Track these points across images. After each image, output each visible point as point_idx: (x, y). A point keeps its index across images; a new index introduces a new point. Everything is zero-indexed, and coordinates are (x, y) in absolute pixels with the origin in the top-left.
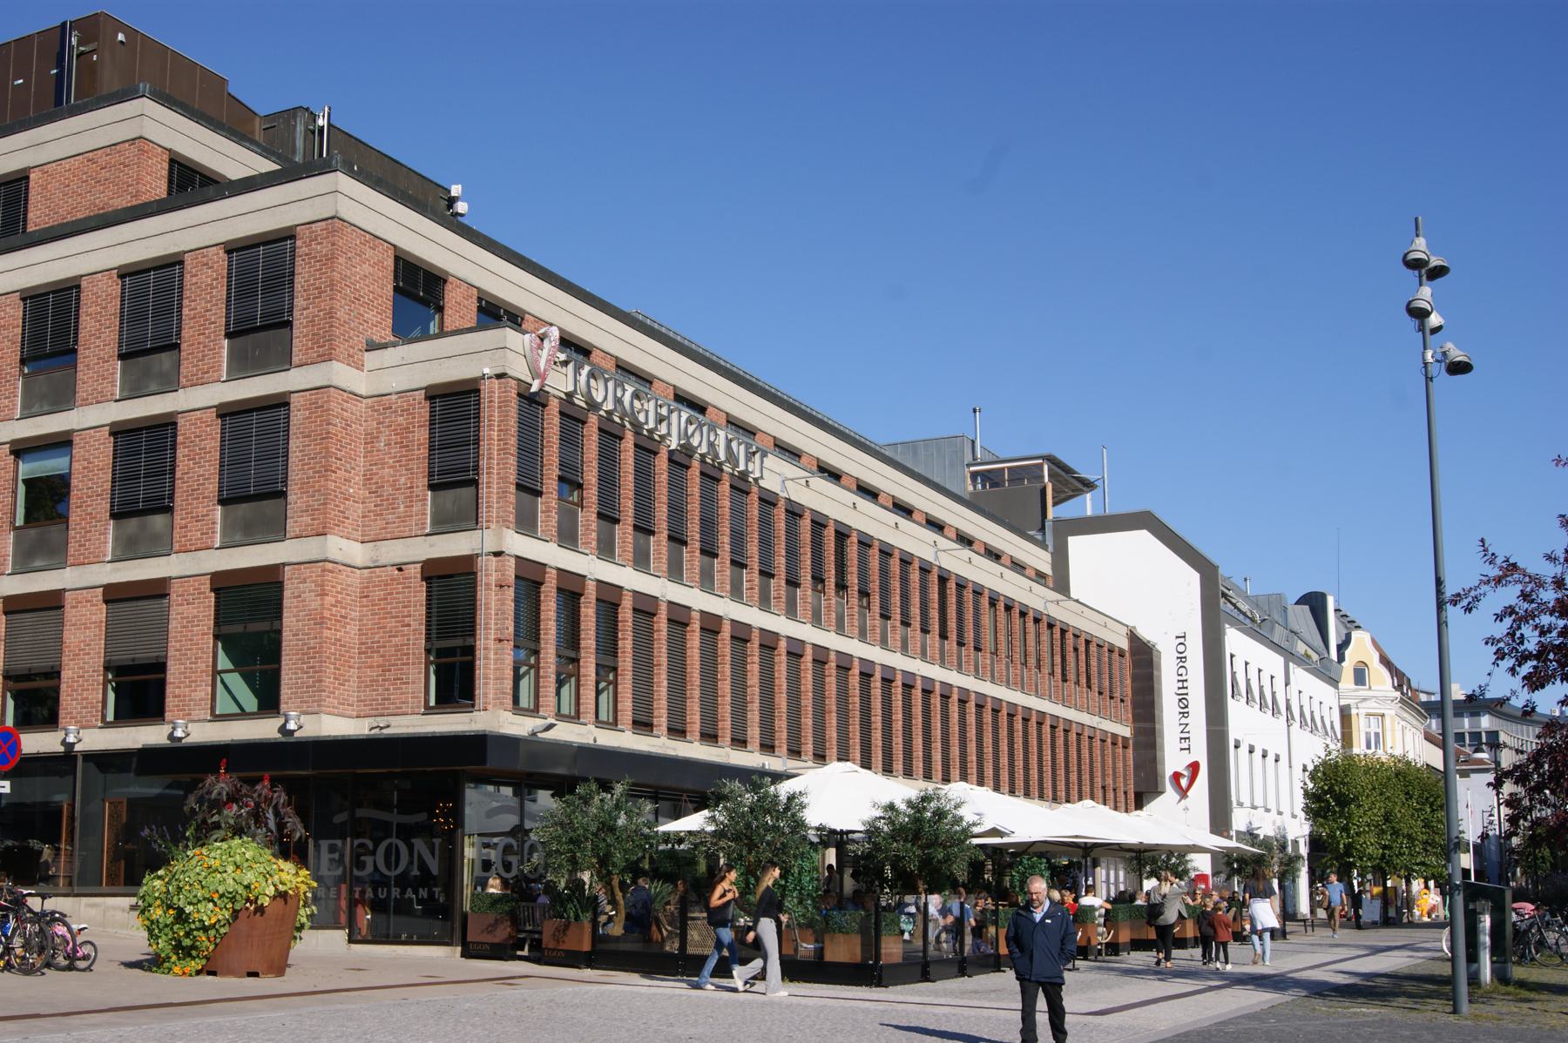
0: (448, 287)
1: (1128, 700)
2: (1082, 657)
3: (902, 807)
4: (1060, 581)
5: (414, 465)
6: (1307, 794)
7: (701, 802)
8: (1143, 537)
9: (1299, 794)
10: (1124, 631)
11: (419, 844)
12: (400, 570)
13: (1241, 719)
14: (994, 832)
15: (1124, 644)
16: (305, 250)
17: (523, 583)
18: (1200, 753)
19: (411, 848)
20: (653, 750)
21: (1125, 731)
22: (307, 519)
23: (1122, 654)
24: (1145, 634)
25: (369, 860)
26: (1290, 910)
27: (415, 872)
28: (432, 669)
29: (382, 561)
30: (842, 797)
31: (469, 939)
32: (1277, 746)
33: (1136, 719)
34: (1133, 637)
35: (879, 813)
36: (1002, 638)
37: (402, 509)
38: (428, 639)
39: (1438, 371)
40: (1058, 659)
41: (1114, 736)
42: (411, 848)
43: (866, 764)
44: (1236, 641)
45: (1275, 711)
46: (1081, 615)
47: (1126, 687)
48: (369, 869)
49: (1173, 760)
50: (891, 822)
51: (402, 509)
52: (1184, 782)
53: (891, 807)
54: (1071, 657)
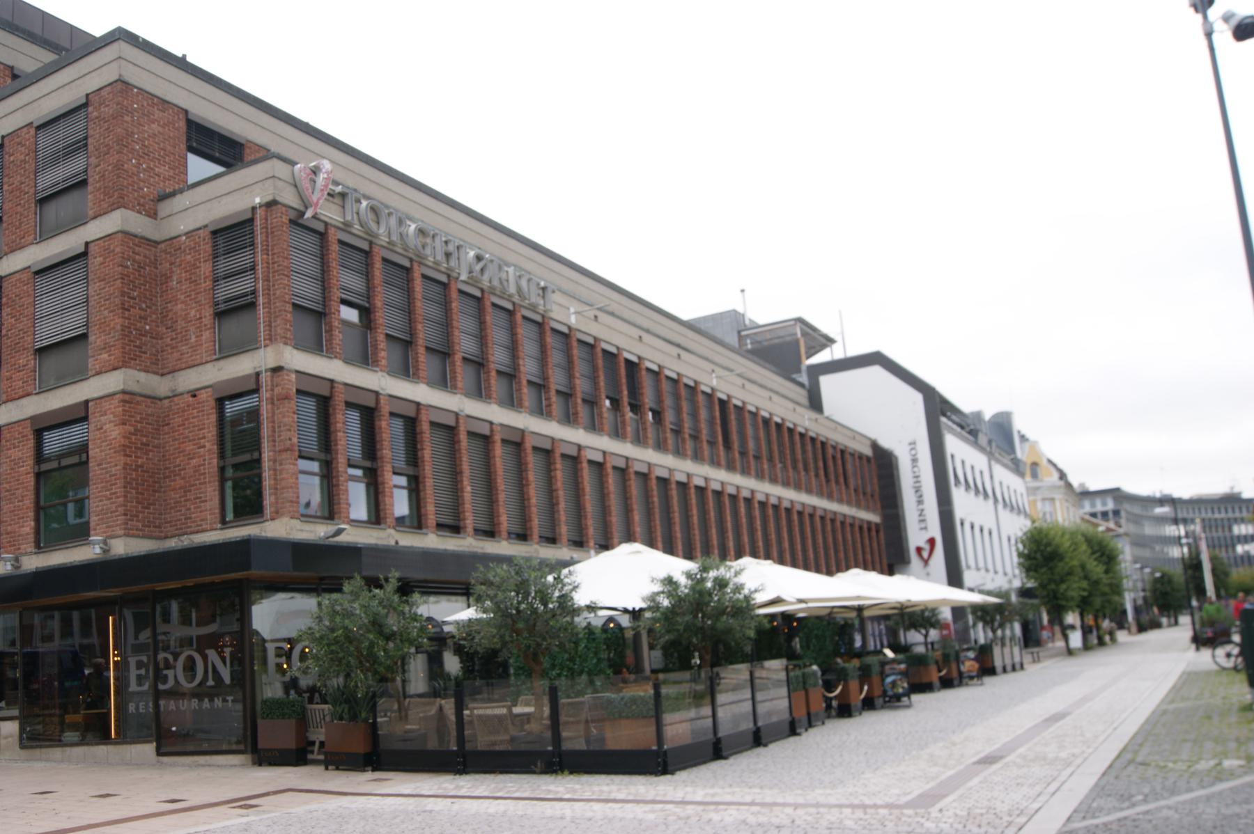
0: (247, 151)
1: (877, 497)
2: (840, 462)
3: (683, 580)
4: (815, 403)
5: (202, 298)
6: (1020, 555)
7: (463, 590)
8: (876, 371)
9: (1015, 554)
10: (868, 443)
11: (212, 654)
12: (194, 396)
13: (963, 504)
14: (777, 601)
15: (868, 451)
16: (95, 114)
17: (253, 380)
18: (935, 531)
19: (205, 658)
20: (380, 542)
21: (874, 518)
22: (105, 356)
23: (868, 459)
24: (885, 443)
25: (170, 673)
26: (325, 482)
27: (211, 683)
28: (229, 484)
29: (180, 390)
30: (620, 580)
31: (260, 746)
32: (989, 523)
33: (883, 507)
34: (875, 446)
35: (657, 588)
36: (775, 447)
37: (193, 339)
38: (222, 455)
39: (1223, 36)
40: (821, 464)
41: (869, 523)
42: (205, 658)
43: (651, 543)
44: (954, 445)
45: (986, 496)
46: (835, 430)
47: (873, 486)
48: (171, 683)
49: (915, 537)
50: (669, 595)
51: (193, 339)
52: (925, 554)
53: (669, 581)
54: (830, 463)
